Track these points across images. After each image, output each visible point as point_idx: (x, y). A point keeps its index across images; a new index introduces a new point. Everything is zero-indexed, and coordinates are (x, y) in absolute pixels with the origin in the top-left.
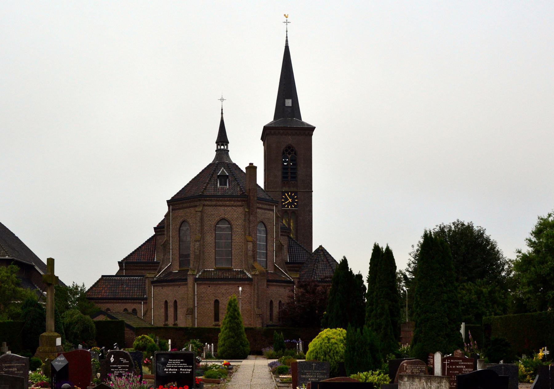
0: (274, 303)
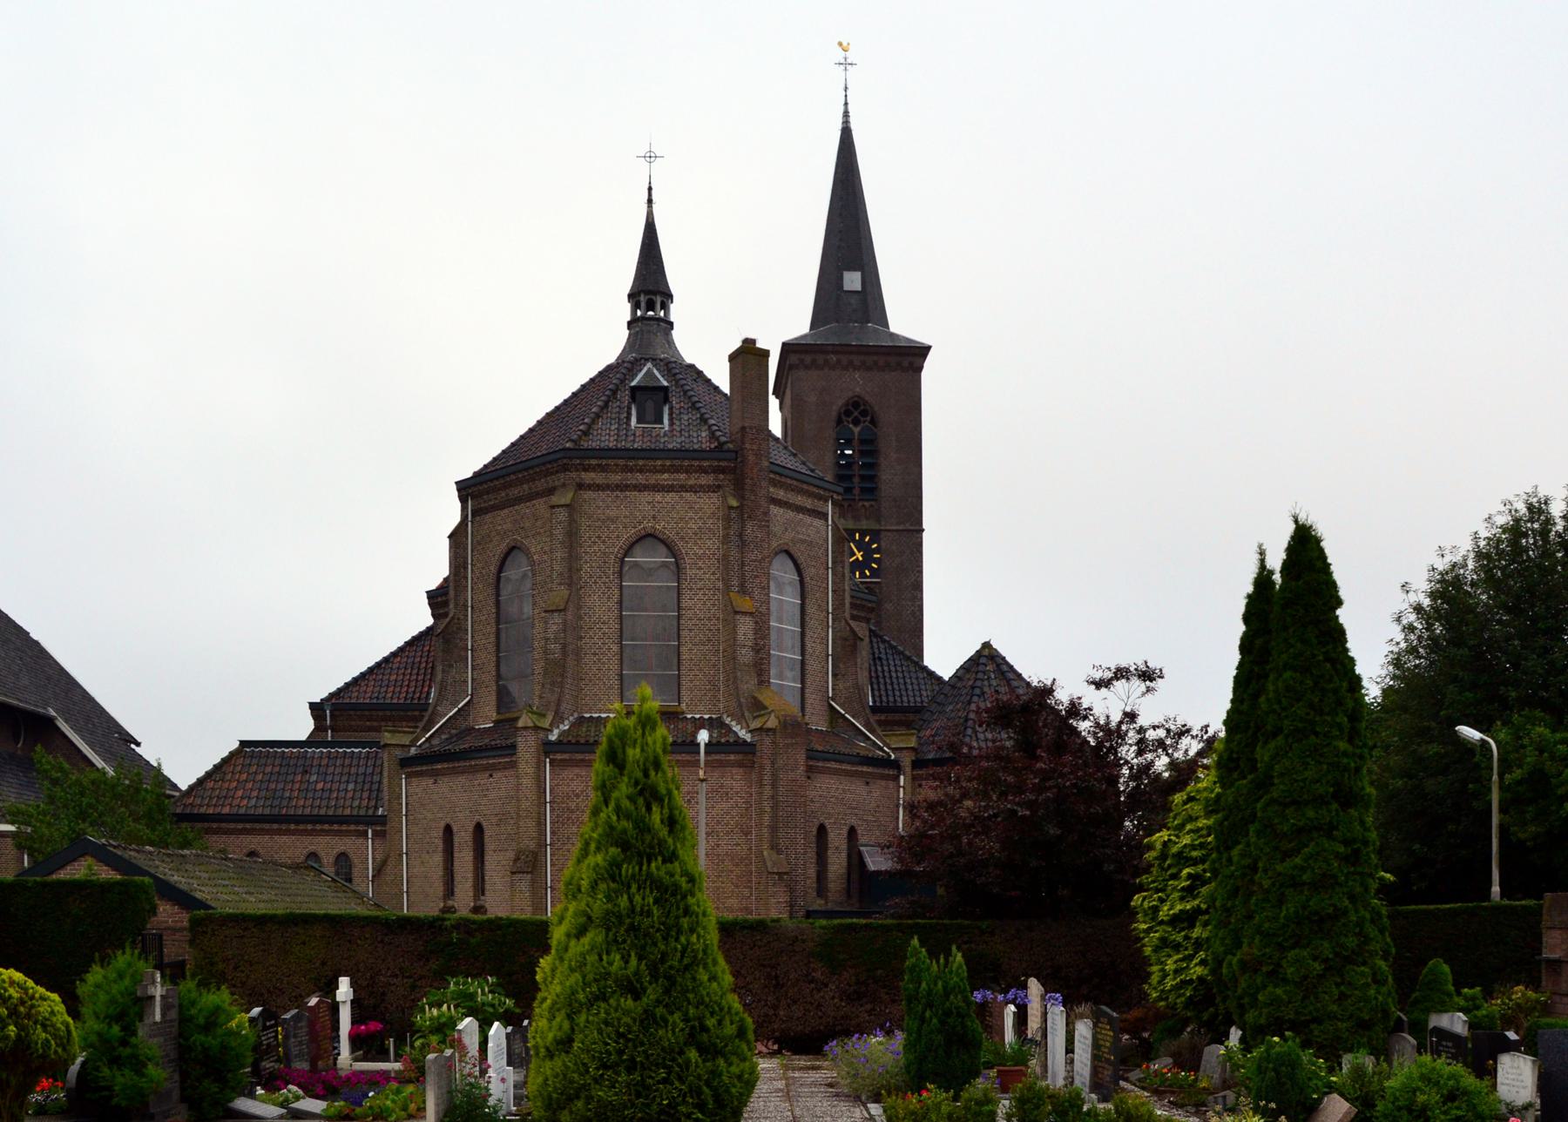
0: (831, 835)
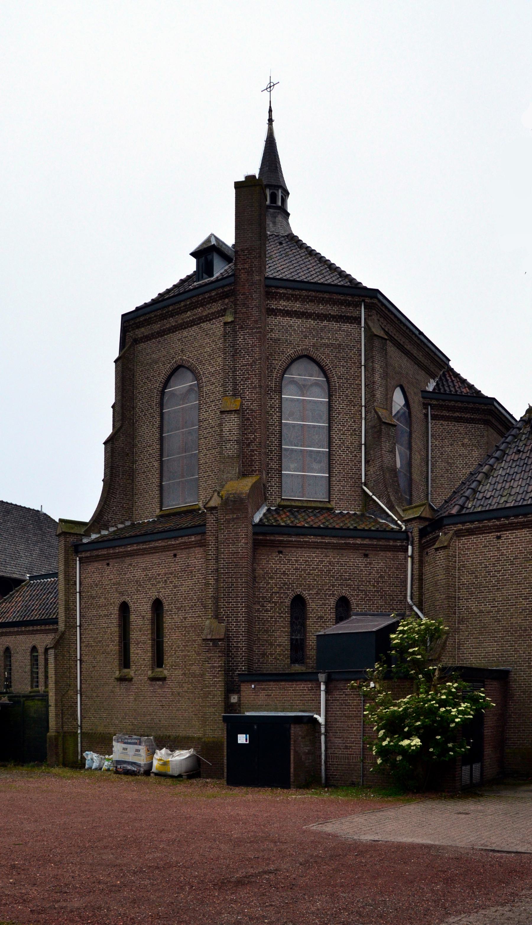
0: (312, 605)
